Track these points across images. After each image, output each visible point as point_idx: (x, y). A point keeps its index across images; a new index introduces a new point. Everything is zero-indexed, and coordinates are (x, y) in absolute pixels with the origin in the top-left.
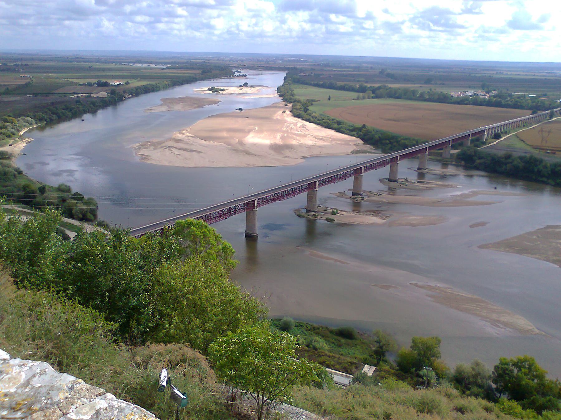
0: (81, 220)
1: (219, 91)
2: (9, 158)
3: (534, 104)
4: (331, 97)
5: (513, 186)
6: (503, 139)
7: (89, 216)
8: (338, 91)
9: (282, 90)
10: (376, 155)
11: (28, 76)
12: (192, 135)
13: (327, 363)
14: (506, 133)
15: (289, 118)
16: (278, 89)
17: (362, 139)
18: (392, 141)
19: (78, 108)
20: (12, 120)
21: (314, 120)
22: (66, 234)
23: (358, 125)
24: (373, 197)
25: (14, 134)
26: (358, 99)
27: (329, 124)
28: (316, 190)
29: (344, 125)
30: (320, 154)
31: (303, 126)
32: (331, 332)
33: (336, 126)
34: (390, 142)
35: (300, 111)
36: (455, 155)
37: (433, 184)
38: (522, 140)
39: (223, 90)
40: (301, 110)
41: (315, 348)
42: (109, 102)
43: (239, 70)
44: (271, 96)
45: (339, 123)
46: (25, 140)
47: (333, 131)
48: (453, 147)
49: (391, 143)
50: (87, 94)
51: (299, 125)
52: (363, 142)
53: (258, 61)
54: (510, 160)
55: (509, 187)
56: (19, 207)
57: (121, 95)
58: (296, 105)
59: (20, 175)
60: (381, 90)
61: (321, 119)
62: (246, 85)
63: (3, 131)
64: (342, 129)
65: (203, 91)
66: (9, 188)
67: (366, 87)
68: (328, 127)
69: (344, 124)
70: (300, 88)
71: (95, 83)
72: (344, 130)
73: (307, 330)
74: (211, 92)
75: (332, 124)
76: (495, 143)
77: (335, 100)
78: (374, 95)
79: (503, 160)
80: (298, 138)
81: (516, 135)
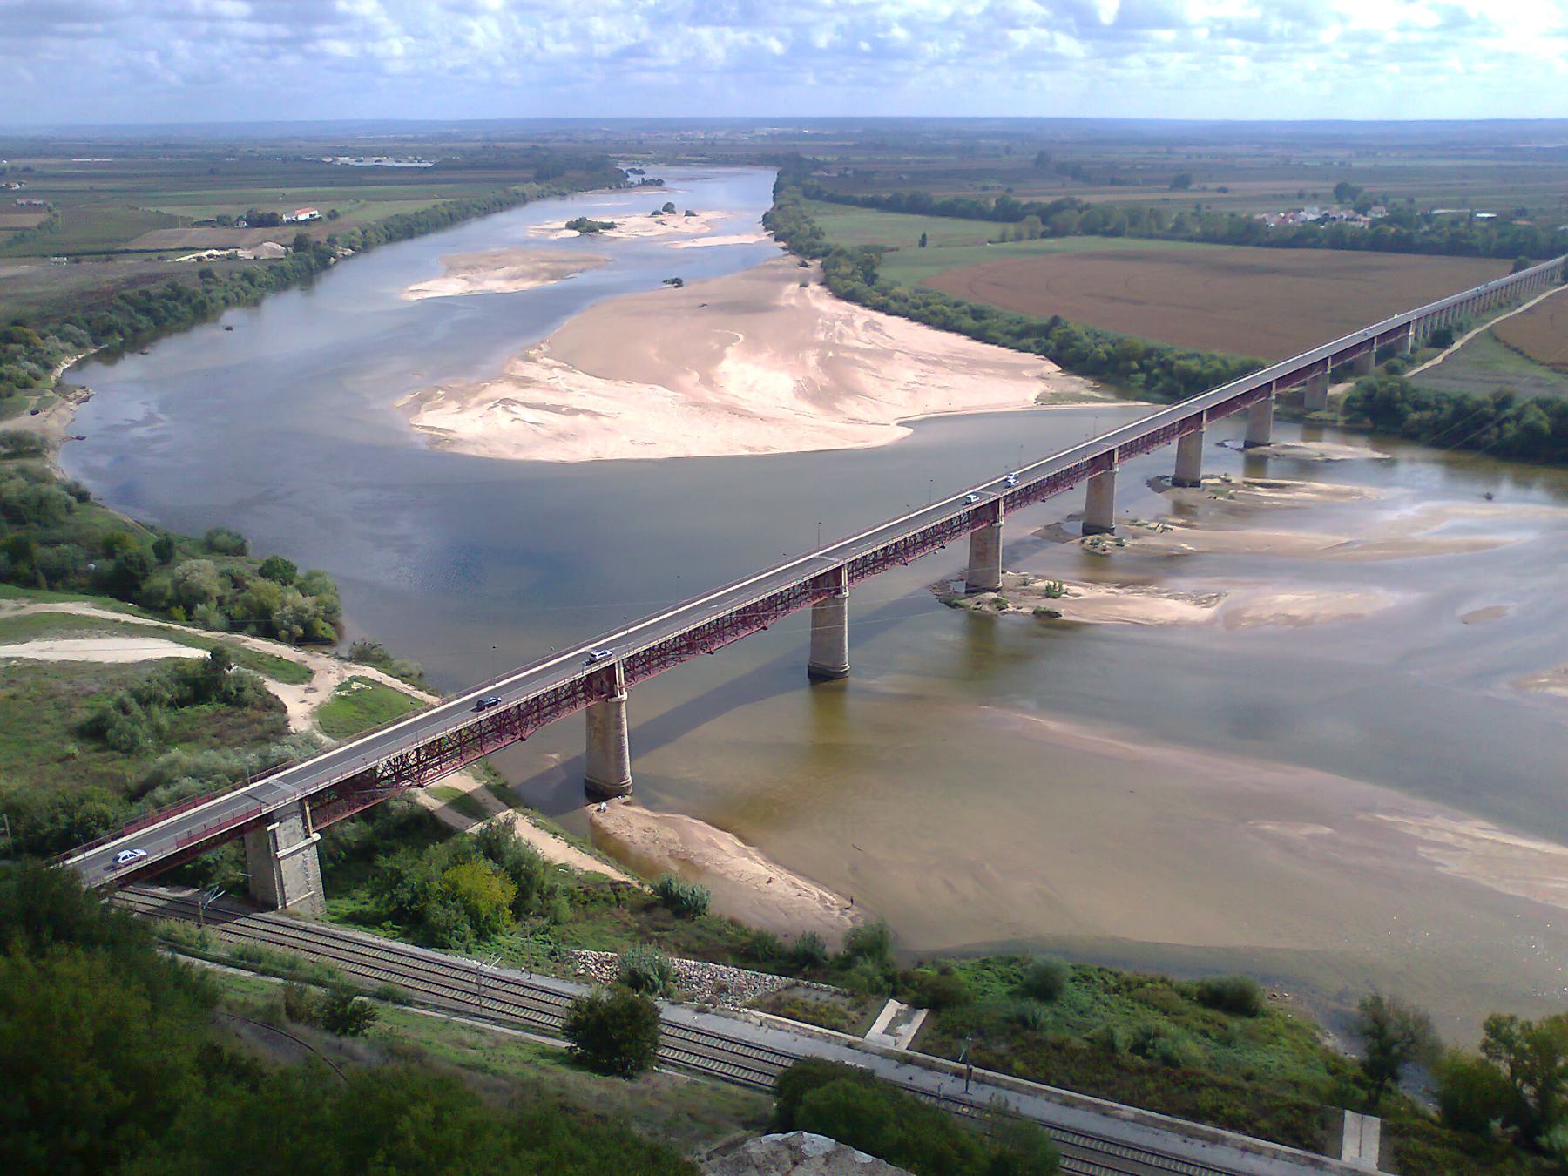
0: (299, 642)
1: (601, 231)
2: (36, 453)
3: (1507, 240)
4: (928, 235)
5: (1523, 482)
6: (1457, 346)
7: (324, 629)
8: (1275, 250)
9: (779, 219)
10: (1144, 414)
11: (41, 202)
12: (558, 364)
13: (1226, 1111)
14: (1462, 329)
15: (828, 305)
16: (767, 220)
17: (1055, 360)
18: (1146, 361)
19: (208, 291)
20: (26, 335)
21: (902, 308)
22: (269, 693)
23: (1039, 319)
24: (1153, 539)
25: (37, 378)
26: (1003, 239)
27: (948, 317)
28: (997, 524)
29: (995, 320)
30: (948, 408)
31: (871, 326)
32: (1183, 994)
33: (968, 322)
34: (1140, 364)
35: (854, 281)
36: (1342, 402)
37: (1308, 489)
38: (1515, 349)
39: (610, 226)
40: (855, 277)
41: (1167, 1060)
42: (294, 271)
43: (637, 168)
44: (751, 239)
45: (977, 314)
46: (71, 396)
47: (962, 337)
48: (1337, 378)
49: (1143, 369)
50: (223, 249)
51: (859, 323)
52: (1060, 369)
53: (881, 147)
54: (1510, 412)
55: (1506, 488)
56: (103, 607)
57: (322, 251)
58: (836, 265)
59: (85, 506)
60: (1065, 214)
61: (921, 302)
62: (669, 208)
63: (5, 369)
64: (990, 333)
65: (552, 230)
66: (64, 547)
67: (1017, 204)
68: (946, 326)
69: (993, 318)
70: (826, 214)
71: (241, 217)
72: (999, 335)
73: (1106, 992)
74: (576, 233)
75: (957, 318)
76: (1439, 359)
77: (940, 246)
78: (1047, 228)
79: (1491, 410)
80: (868, 362)
81: (1490, 331)
